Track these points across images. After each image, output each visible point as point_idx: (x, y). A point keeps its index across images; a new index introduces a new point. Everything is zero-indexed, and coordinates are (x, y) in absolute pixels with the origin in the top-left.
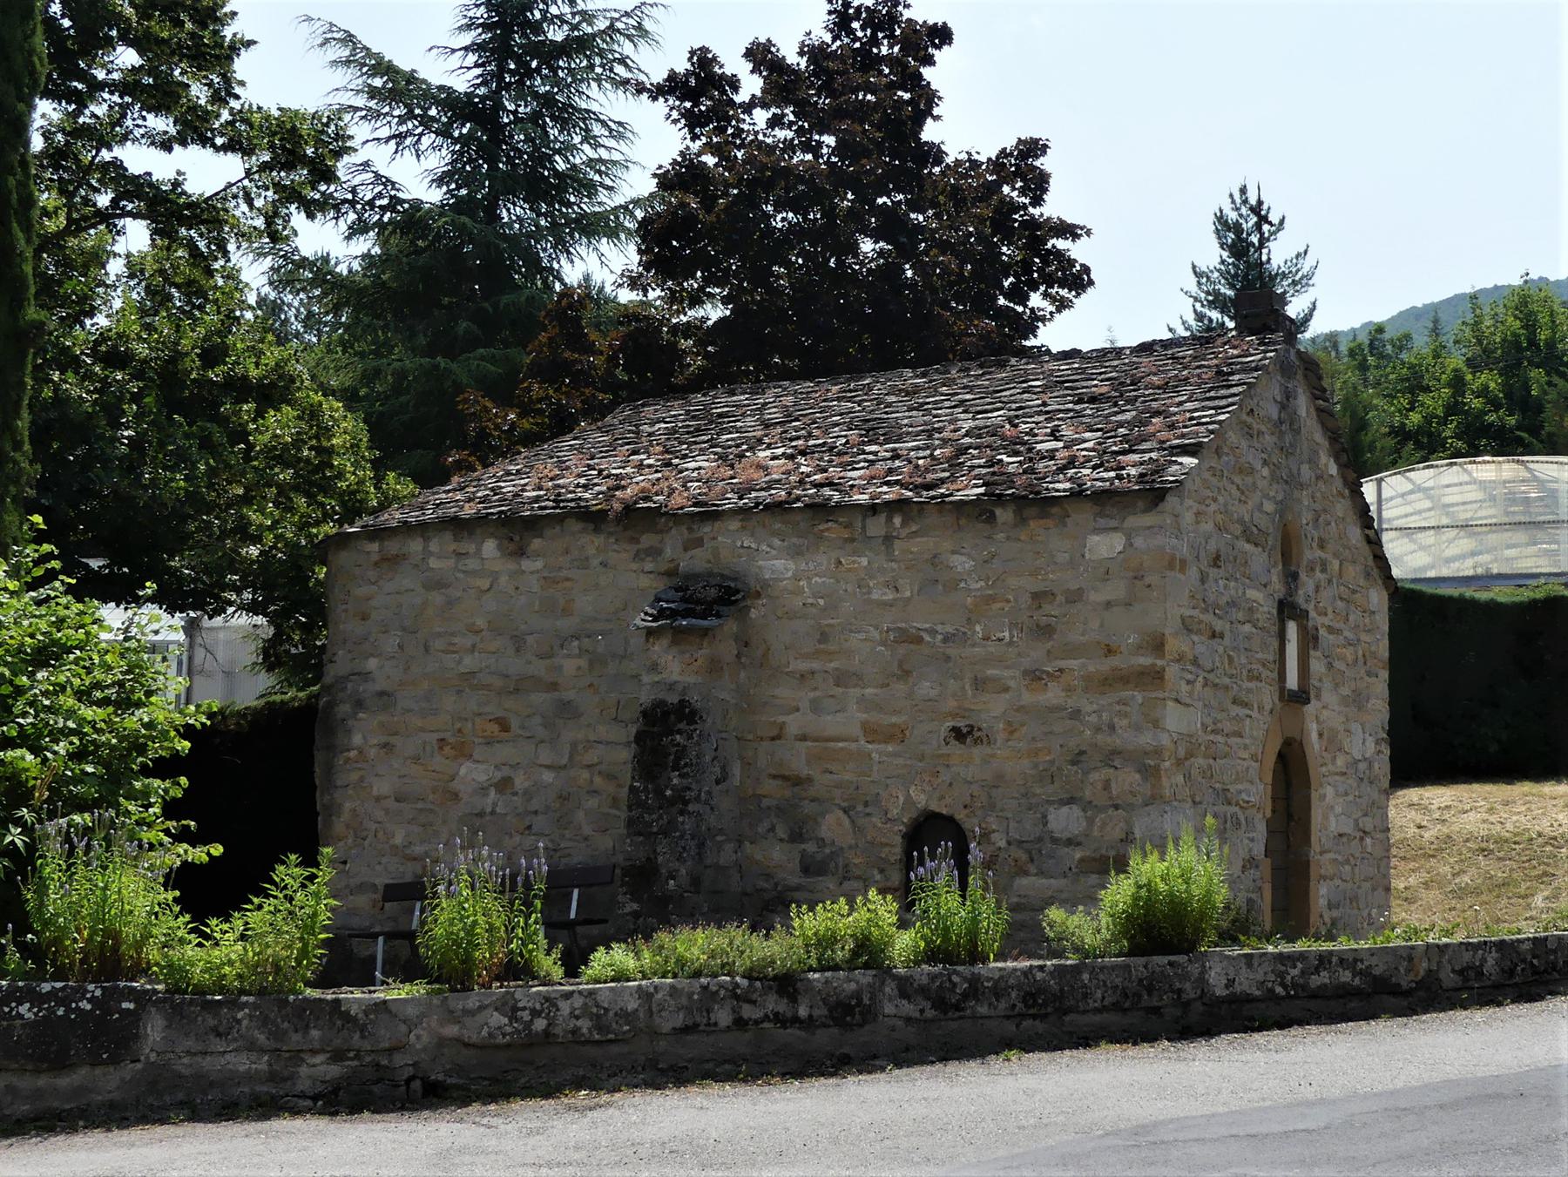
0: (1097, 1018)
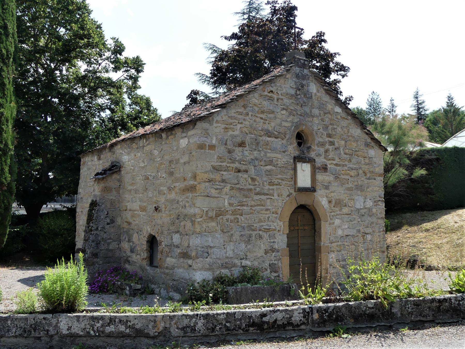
0: (15, 340)
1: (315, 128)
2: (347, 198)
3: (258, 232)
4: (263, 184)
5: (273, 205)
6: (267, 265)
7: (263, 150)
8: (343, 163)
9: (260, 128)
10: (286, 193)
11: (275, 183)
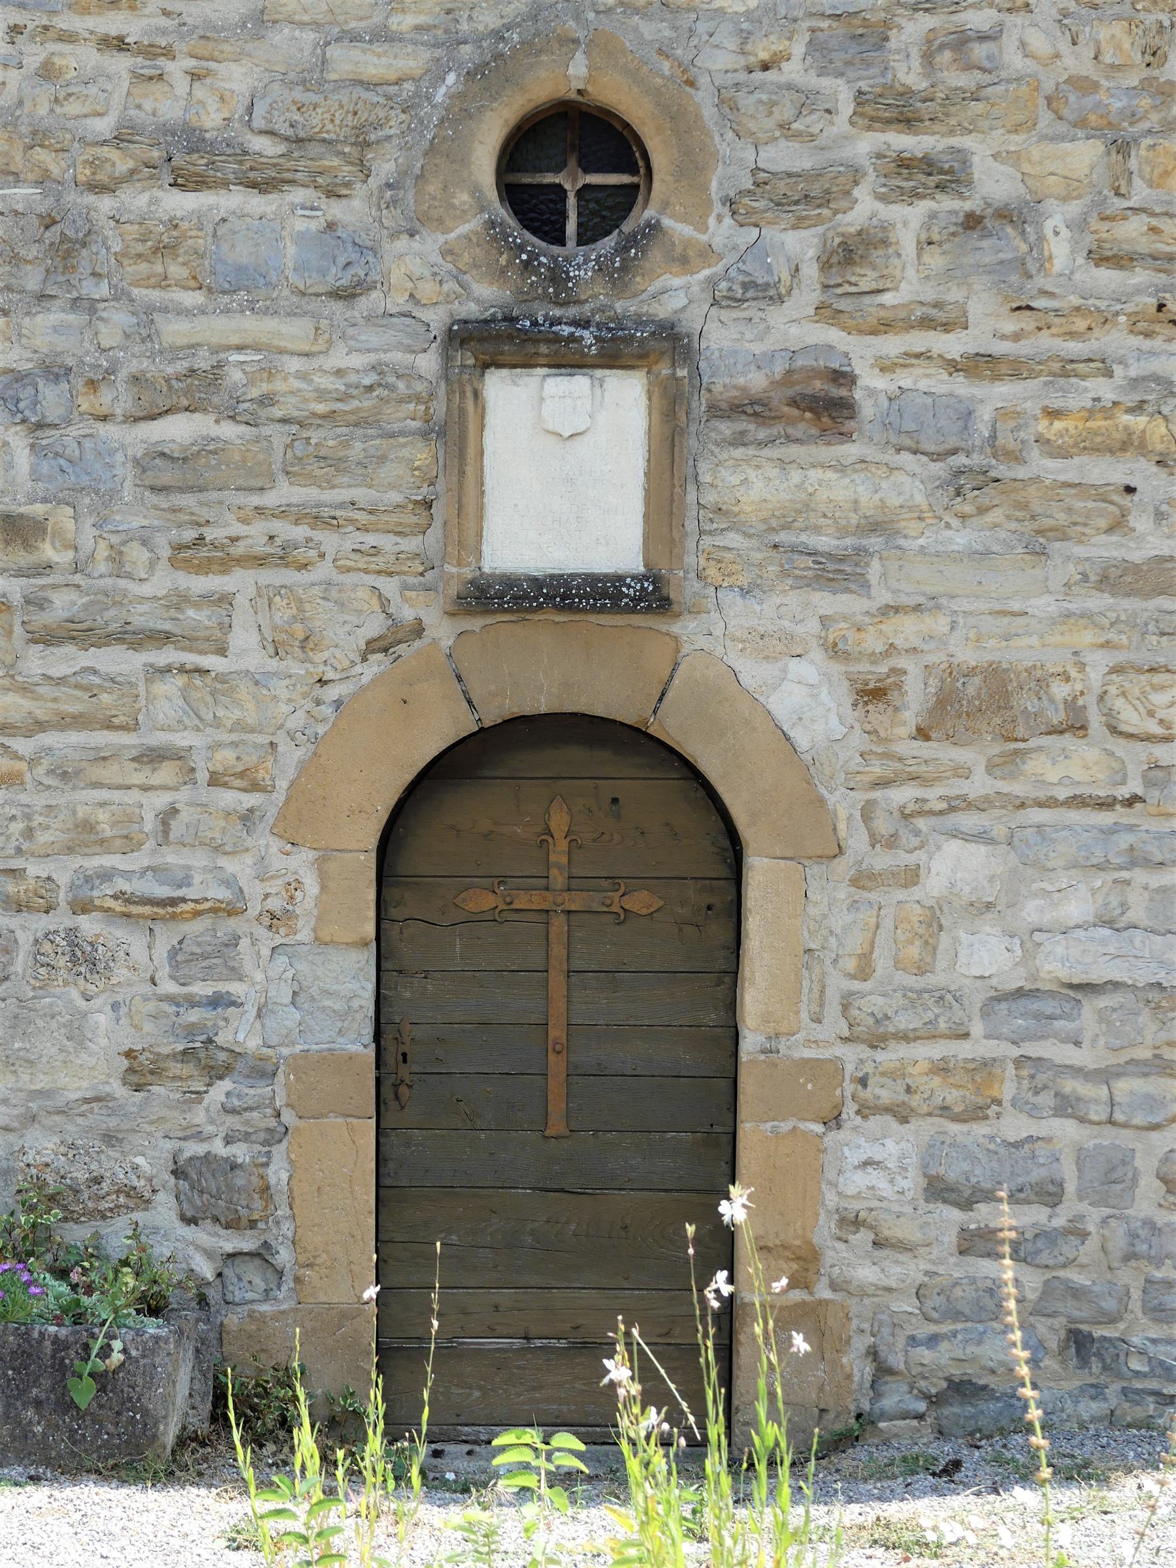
1: (720, 61)
2: (1099, 663)
3: (61, 920)
4: (117, 557)
5: (217, 723)
6: (147, 1160)
7: (120, 294)
8: (1074, 348)
9: (104, 126)
10: (346, 631)
11: (239, 549)
